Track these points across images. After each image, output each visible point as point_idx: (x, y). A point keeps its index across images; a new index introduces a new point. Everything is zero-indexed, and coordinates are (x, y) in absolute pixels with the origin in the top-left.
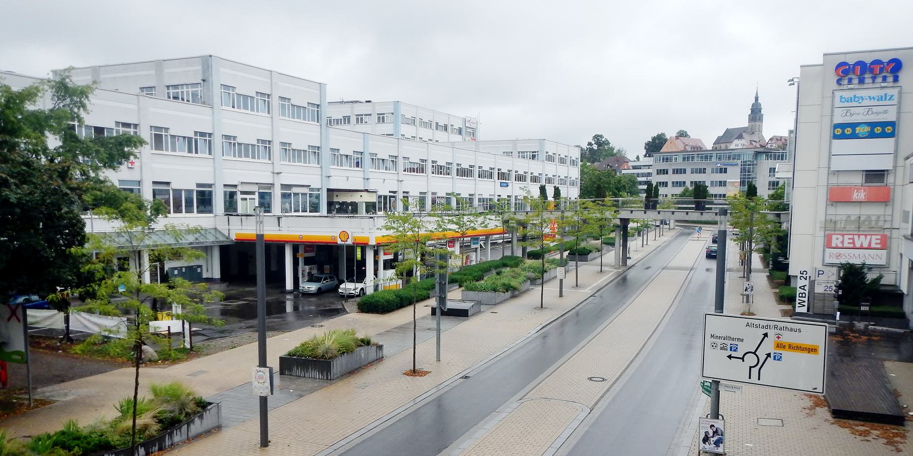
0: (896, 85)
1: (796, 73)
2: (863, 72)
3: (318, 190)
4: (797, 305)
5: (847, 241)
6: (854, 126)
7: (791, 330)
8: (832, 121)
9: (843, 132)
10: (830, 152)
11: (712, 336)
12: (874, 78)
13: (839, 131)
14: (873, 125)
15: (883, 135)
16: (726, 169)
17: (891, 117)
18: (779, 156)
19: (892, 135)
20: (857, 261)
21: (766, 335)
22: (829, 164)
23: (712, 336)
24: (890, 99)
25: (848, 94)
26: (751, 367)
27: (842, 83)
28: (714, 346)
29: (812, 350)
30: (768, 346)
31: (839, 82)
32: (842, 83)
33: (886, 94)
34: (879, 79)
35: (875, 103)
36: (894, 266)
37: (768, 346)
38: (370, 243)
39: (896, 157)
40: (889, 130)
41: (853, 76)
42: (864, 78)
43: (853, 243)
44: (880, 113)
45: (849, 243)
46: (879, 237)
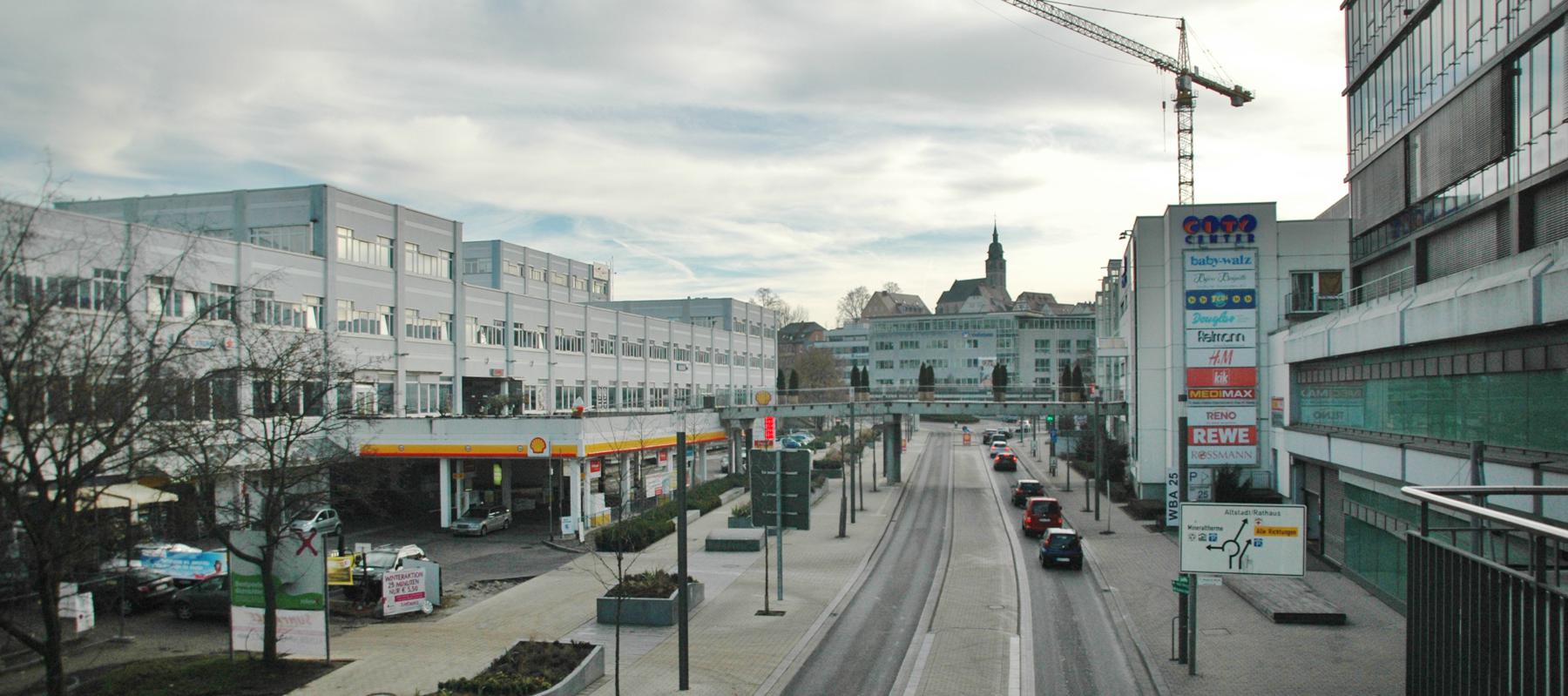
0: (1252, 245)
1: (1129, 225)
2: (1214, 230)
3: (450, 379)
4: (1168, 517)
5: (1210, 436)
6: (1209, 293)
7: (1271, 514)
8: (1184, 287)
9: (1198, 298)
10: (1184, 326)
11: (1189, 527)
12: (1227, 237)
13: (1192, 300)
14: (1230, 293)
15: (1242, 305)
16: (917, 343)
17: (1249, 284)
18: (1047, 322)
19: (1252, 305)
20: (1232, 461)
21: (1245, 521)
22: (1184, 341)
23: (1189, 527)
24: (1247, 262)
25: (1199, 255)
26: (1231, 557)
27: (1192, 240)
28: (1192, 537)
29: (1291, 533)
30: (1250, 532)
31: (1188, 240)
32: (1192, 240)
33: (1242, 257)
34: (1233, 239)
35: (1228, 266)
36: (1266, 466)
37: (1250, 532)
38: (579, 455)
39: (1258, 332)
40: (1248, 299)
41: (1204, 234)
42: (1216, 236)
43: (1218, 438)
44: (1237, 279)
45: (1214, 438)
46: (1247, 430)
